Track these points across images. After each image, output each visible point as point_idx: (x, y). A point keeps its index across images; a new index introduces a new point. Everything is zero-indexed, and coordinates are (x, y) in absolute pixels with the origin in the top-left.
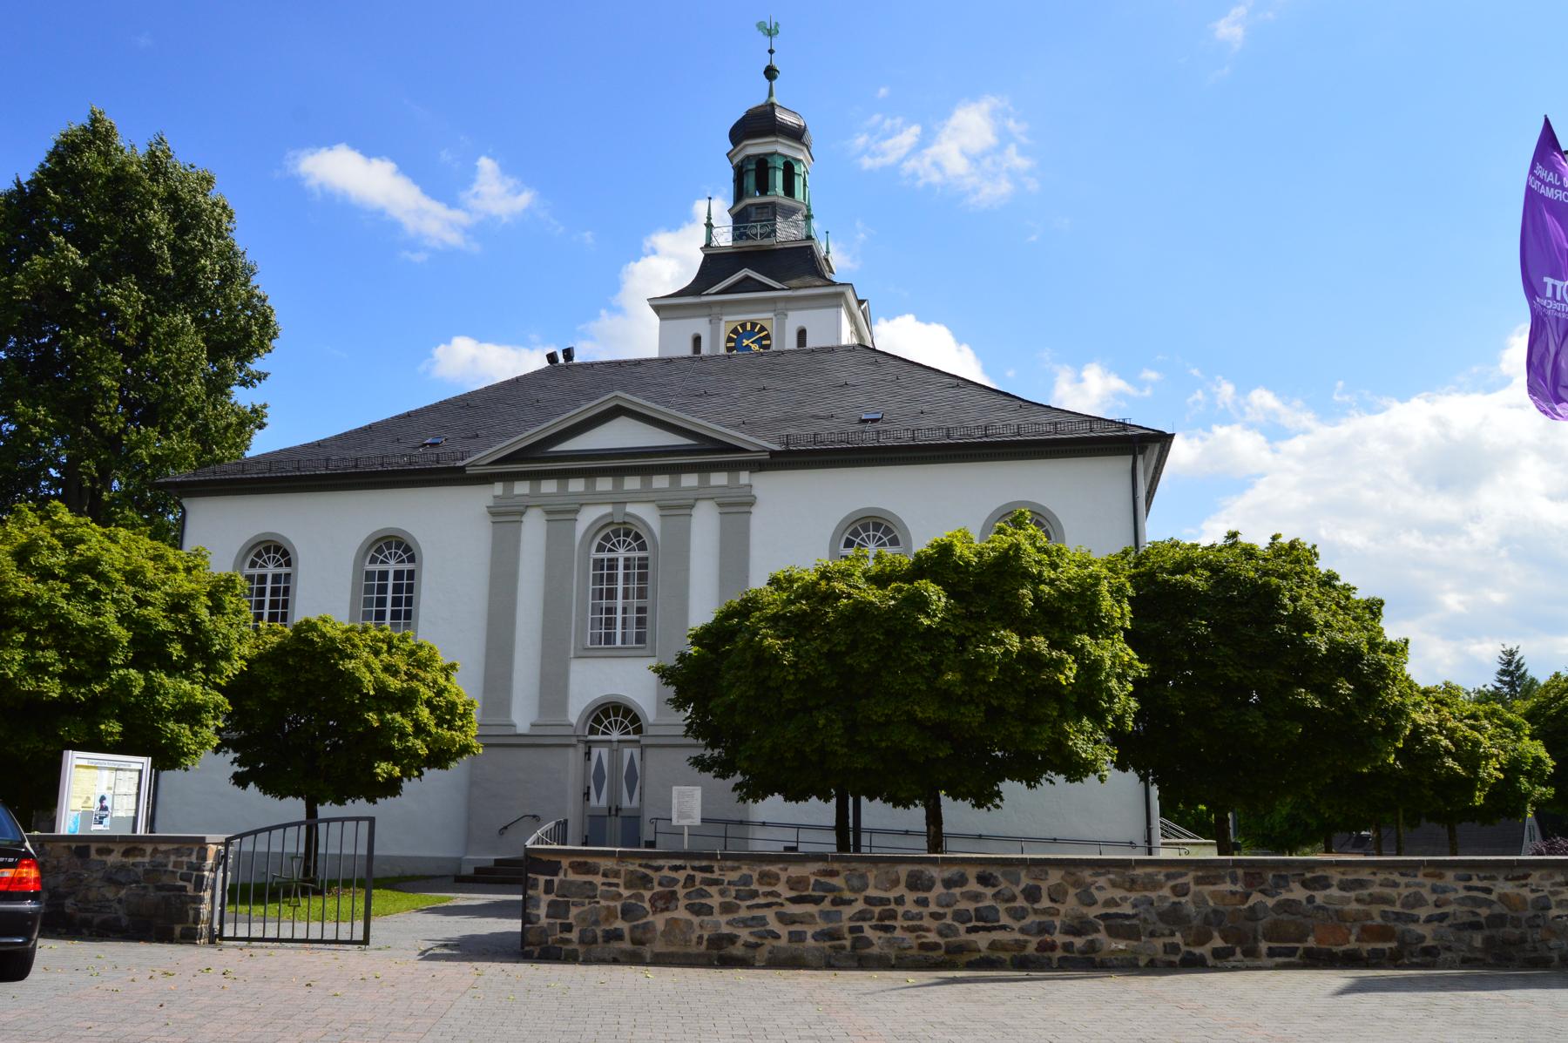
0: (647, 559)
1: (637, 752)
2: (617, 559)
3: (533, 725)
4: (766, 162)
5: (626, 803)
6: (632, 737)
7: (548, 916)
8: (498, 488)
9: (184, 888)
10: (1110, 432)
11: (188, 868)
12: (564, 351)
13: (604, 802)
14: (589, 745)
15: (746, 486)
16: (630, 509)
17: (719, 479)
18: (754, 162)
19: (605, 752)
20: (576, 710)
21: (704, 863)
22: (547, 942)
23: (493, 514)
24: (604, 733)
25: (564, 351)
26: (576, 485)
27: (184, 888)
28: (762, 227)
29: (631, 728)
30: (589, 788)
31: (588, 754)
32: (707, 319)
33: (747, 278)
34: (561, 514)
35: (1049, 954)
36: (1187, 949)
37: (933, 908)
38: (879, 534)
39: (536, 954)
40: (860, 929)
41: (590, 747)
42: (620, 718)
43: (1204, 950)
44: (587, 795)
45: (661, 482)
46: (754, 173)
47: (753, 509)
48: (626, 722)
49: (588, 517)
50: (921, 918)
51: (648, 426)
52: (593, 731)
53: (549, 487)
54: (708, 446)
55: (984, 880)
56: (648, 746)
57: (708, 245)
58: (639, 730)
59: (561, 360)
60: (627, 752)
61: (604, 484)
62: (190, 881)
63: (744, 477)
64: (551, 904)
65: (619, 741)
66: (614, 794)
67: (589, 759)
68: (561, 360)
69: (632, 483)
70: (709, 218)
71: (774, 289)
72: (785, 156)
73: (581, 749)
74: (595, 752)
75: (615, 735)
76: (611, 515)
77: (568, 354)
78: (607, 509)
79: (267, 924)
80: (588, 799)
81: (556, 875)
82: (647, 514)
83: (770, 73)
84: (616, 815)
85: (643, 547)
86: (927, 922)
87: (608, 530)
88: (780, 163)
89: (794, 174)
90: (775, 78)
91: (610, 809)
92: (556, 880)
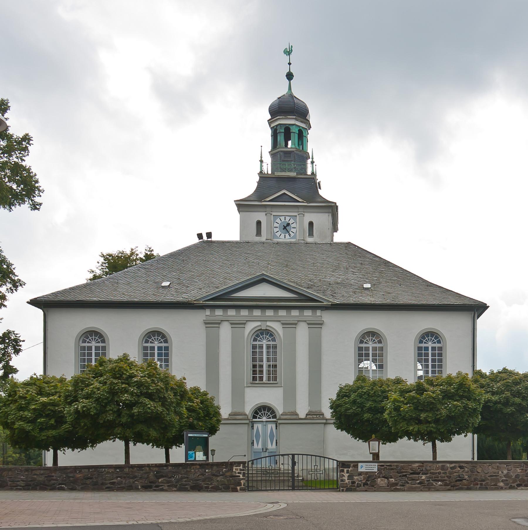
0: (276, 344)
1: (274, 426)
2: (263, 344)
3: (229, 415)
4: (290, 129)
5: (269, 446)
6: (272, 420)
7: (348, 480)
8: (208, 312)
9: (239, 476)
10: (467, 302)
11: (240, 470)
12: (207, 233)
13: (260, 446)
14: (253, 423)
15: (319, 316)
16: (268, 324)
17: (308, 313)
18: (283, 128)
19: (260, 426)
20: (248, 409)
21: (389, 464)
22: (348, 487)
23: (206, 323)
24: (259, 418)
25: (207, 233)
26: (244, 313)
27: (239, 476)
28: (288, 165)
29: (271, 416)
30: (253, 440)
31: (253, 427)
32: (264, 213)
33: (284, 194)
34: (240, 324)
35: (476, 486)
36: (510, 485)
37: (448, 475)
38: (374, 338)
39: (345, 490)
40: (429, 480)
41: (253, 424)
42: (263, 412)
43: (515, 485)
44: (253, 443)
45: (282, 313)
46: (283, 134)
47: (323, 327)
48: (266, 412)
49: (251, 326)
50: (445, 478)
51: (285, 291)
52: (254, 417)
53: (232, 312)
54: (303, 298)
55: (461, 467)
56: (280, 424)
57: (261, 172)
58: (275, 417)
59: (205, 238)
60: (269, 426)
61: (257, 313)
62: (241, 474)
63: (319, 313)
64: (348, 476)
65: (266, 421)
66: (265, 443)
67: (253, 429)
68: (205, 238)
69: (270, 313)
70: (261, 157)
71: (298, 202)
72: (299, 126)
73: (250, 425)
74: (255, 426)
75: (264, 419)
76: (260, 326)
77: (209, 235)
78: (259, 323)
79: (280, 483)
80: (253, 445)
81: (350, 468)
82: (277, 327)
83: (290, 76)
84: (266, 452)
85: (274, 340)
86: (446, 478)
87: (258, 332)
88: (296, 130)
89: (303, 136)
90: (292, 79)
91: (263, 449)
92: (350, 469)
